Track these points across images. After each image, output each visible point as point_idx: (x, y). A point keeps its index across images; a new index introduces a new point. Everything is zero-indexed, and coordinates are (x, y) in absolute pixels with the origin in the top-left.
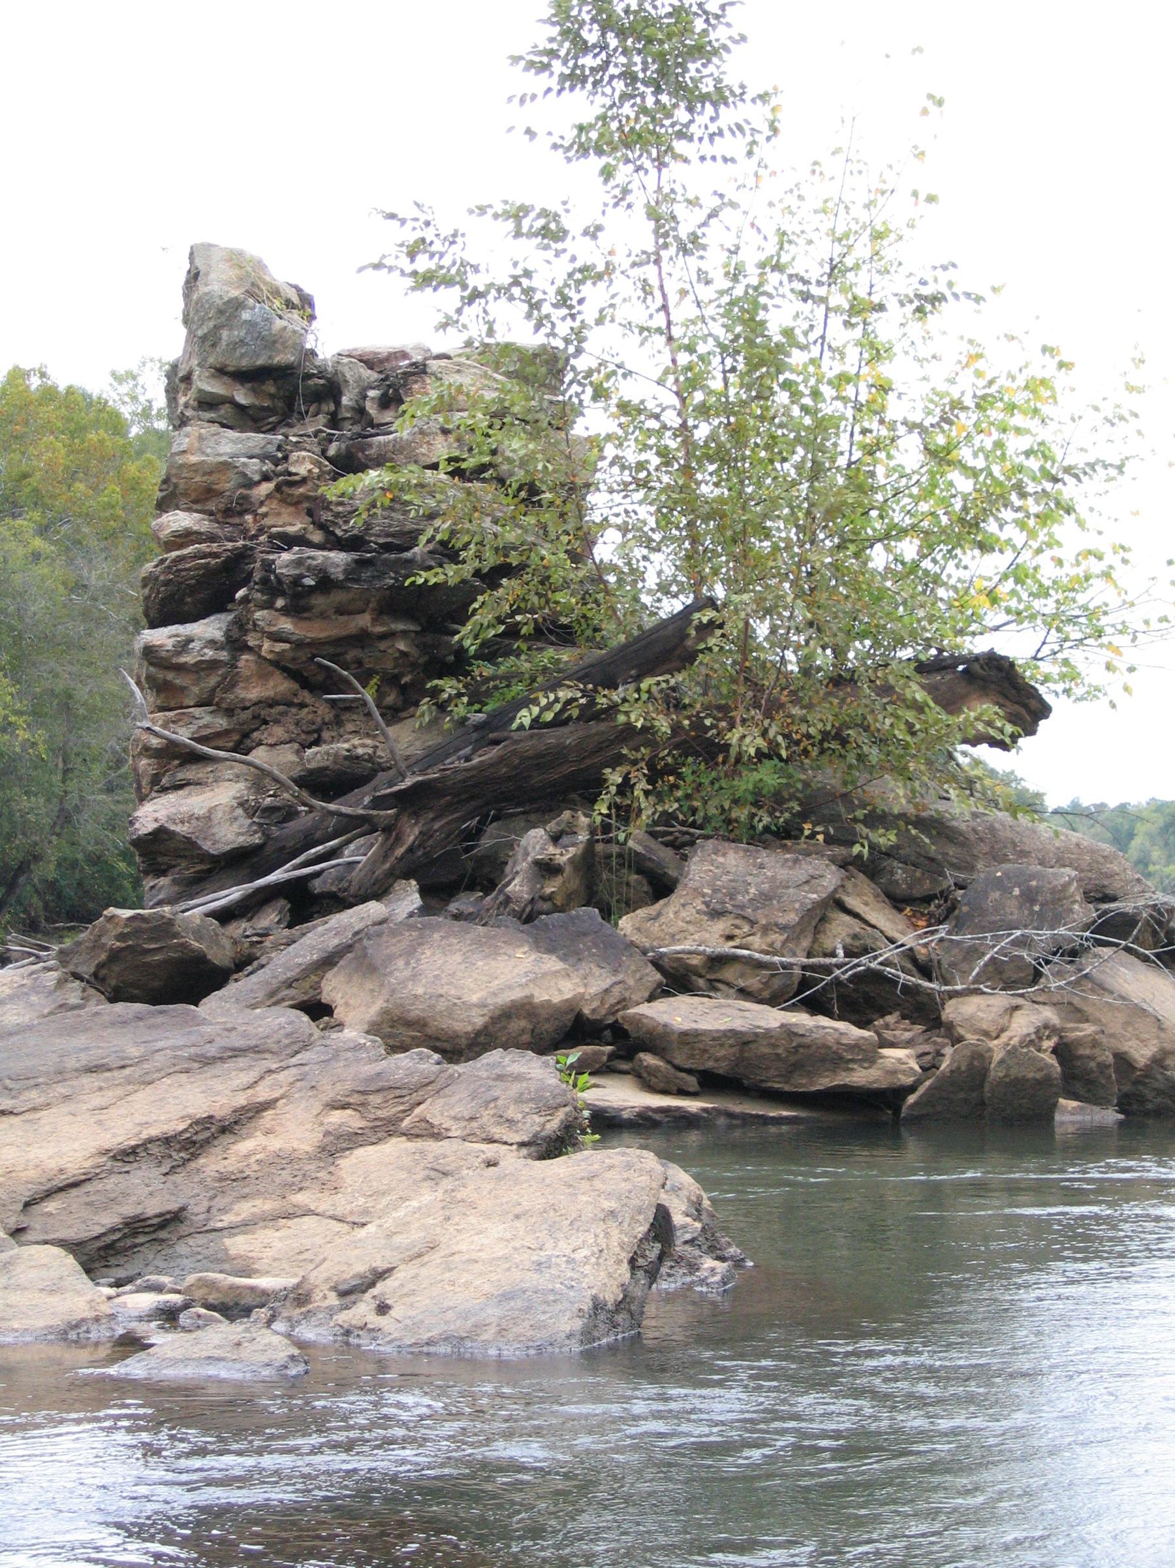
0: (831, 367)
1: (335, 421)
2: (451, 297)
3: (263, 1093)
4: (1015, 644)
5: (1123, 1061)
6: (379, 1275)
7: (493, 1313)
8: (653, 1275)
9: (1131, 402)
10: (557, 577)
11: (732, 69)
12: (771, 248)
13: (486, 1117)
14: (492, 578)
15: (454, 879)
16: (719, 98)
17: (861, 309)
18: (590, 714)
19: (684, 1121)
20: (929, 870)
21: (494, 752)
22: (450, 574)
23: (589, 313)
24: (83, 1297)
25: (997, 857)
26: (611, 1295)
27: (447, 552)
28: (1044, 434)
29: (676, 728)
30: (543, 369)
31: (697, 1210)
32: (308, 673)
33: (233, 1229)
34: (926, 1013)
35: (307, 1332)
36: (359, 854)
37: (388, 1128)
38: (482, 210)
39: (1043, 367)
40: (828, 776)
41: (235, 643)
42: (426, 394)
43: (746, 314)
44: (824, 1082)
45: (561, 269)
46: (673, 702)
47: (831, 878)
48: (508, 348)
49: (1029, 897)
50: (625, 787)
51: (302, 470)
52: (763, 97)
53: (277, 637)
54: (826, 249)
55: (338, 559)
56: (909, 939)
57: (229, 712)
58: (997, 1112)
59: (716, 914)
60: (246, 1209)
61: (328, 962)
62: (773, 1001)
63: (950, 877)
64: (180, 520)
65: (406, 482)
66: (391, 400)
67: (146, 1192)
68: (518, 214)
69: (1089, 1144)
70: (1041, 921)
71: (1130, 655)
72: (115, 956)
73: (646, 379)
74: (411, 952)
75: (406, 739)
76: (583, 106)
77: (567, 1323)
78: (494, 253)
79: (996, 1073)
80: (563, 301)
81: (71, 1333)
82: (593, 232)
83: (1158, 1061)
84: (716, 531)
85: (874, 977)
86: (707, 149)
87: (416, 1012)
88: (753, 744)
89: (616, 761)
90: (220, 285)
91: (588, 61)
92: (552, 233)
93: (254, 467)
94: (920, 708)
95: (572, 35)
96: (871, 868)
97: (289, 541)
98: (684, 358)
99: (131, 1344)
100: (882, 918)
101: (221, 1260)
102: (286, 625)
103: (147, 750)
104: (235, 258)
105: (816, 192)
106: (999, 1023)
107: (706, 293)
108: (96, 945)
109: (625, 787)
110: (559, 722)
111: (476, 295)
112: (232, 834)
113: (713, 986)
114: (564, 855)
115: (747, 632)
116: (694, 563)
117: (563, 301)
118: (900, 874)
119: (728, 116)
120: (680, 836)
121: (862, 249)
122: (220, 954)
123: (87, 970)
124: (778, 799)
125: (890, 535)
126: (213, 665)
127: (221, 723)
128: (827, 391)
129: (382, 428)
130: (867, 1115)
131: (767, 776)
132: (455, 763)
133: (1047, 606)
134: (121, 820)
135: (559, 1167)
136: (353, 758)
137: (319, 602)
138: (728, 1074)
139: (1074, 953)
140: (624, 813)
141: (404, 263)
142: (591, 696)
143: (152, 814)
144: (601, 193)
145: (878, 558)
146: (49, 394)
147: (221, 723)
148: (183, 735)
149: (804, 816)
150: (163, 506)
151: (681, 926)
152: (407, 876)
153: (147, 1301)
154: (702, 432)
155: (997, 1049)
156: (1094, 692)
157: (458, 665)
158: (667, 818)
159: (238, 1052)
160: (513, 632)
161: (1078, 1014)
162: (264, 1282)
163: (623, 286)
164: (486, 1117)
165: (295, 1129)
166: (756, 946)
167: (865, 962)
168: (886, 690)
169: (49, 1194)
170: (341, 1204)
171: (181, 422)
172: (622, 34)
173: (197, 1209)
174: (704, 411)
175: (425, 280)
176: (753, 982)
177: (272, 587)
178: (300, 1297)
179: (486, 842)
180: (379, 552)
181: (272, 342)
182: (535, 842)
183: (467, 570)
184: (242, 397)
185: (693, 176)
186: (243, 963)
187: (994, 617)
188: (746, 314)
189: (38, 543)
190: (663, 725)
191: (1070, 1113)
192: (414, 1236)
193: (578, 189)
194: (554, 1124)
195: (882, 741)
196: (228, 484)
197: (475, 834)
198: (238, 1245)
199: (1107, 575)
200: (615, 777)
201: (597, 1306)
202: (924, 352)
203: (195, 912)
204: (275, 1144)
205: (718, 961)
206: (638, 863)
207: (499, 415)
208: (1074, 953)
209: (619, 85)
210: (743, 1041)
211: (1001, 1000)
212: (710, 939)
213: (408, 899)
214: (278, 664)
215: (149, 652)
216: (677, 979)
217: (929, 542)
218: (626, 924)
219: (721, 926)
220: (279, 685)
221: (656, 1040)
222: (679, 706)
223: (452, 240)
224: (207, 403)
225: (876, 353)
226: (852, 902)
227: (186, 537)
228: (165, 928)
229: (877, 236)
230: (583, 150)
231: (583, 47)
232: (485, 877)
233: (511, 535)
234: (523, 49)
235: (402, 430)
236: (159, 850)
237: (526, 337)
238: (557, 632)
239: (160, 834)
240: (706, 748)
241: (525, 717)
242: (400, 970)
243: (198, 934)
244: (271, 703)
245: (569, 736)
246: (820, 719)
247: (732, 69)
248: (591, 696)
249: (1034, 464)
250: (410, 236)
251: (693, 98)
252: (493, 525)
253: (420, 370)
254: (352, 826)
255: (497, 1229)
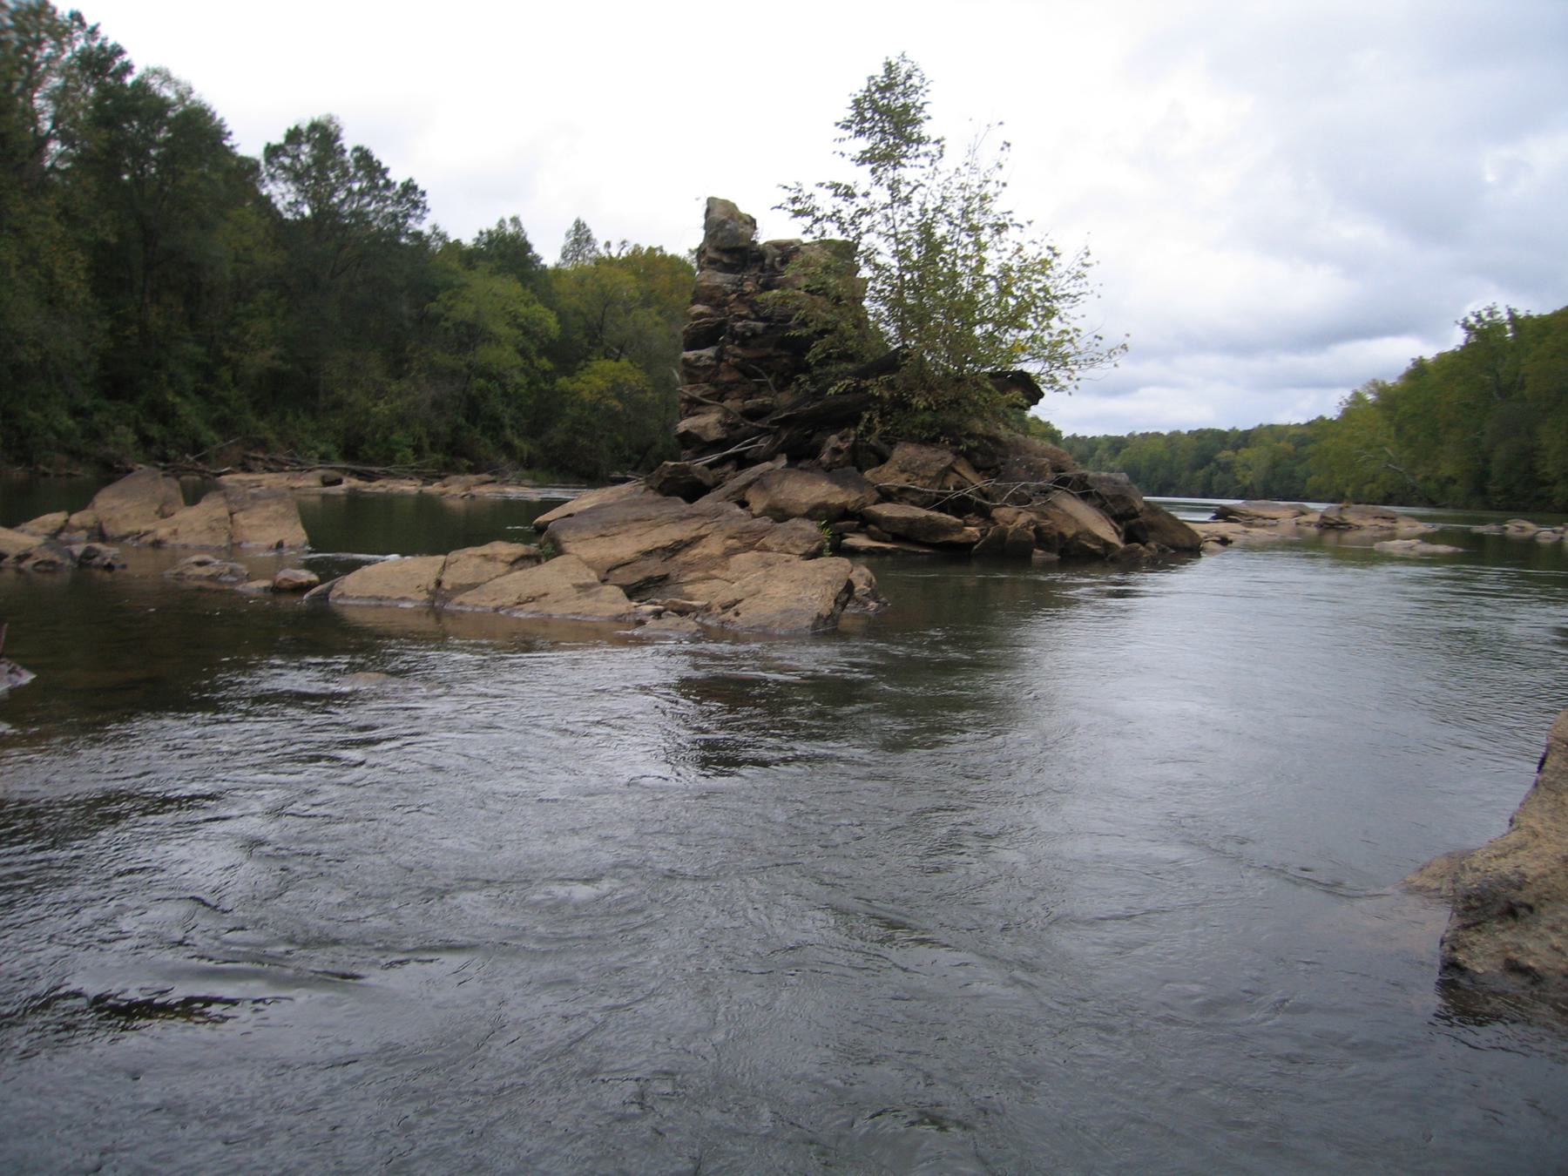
0: (961, 252)
1: (762, 270)
2: (808, 221)
3: (703, 532)
4: (1032, 368)
5: (1062, 535)
6: (738, 602)
7: (779, 617)
8: (844, 606)
9: (1084, 270)
10: (847, 334)
11: (926, 129)
12: (939, 203)
13: (788, 543)
14: (821, 333)
15: (801, 454)
16: (920, 141)
17: (974, 229)
18: (857, 389)
19: (883, 552)
20: (990, 457)
21: (818, 404)
22: (804, 332)
23: (863, 228)
24: (624, 605)
25: (1018, 453)
26: (826, 612)
27: (803, 323)
28: (1048, 283)
29: (892, 396)
30: (846, 251)
31: (870, 583)
32: (745, 370)
33: (687, 583)
34: (985, 513)
35: (709, 622)
36: (764, 443)
37: (749, 547)
38: (821, 185)
39: (1046, 254)
40: (951, 418)
41: (719, 358)
42: (798, 260)
43: (926, 230)
44: (941, 539)
45: (853, 209)
46: (891, 385)
47: (950, 458)
48: (831, 242)
49: (1029, 469)
50: (870, 420)
51: (748, 289)
52: (938, 142)
53: (735, 356)
54: (961, 204)
55: (760, 325)
56: (980, 484)
57: (716, 386)
58: (1009, 553)
59: (903, 471)
60: (692, 576)
61: (749, 485)
62: (924, 506)
63: (999, 460)
64: (699, 308)
65: (791, 293)
66: (784, 262)
67: (655, 568)
68: (835, 186)
69: (1047, 567)
70: (1033, 479)
71: (1078, 374)
72: (667, 480)
73: (886, 258)
74: (780, 482)
75: (785, 398)
76: (864, 144)
77: (807, 622)
78: (826, 202)
79: (1009, 538)
80: (853, 223)
81: (619, 619)
82: (866, 195)
83: (1076, 536)
84: (911, 317)
85: (965, 499)
86: (913, 161)
87: (781, 505)
88: (922, 404)
89: (867, 409)
90: (718, 215)
91: (867, 125)
92: (849, 194)
93: (729, 287)
94: (989, 391)
95: (860, 114)
96: (968, 455)
97: (741, 318)
98: (901, 247)
99: (641, 623)
100: (970, 475)
101: (681, 595)
102: (739, 351)
103: (683, 400)
104: (725, 203)
105: (956, 182)
106: (1014, 518)
107: (911, 220)
108: (660, 476)
109: (870, 420)
110: (845, 392)
111: (817, 221)
112: (714, 434)
113: (900, 500)
114: (844, 446)
115: (922, 359)
116: (903, 332)
117: (853, 223)
118: (979, 458)
119: (922, 149)
120: (891, 440)
121: (976, 204)
122: (709, 481)
123: (656, 485)
124: (931, 426)
125: (982, 322)
126: (709, 366)
127: (712, 390)
128: (959, 262)
129: (781, 273)
130: (960, 553)
131: (927, 417)
132: (803, 408)
133: (1046, 352)
134: (667, 427)
135: (812, 563)
136: (763, 405)
137: (753, 342)
138: (905, 534)
139: (1046, 492)
140: (869, 430)
141: (790, 206)
142: (858, 383)
143: (684, 425)
144: (870, 179)
145: (978, 331)
146: (664, 257)
147: (712, 390)
148: (697, 394)
149: (941, 434)
150: (693, 303)
151: (888, 476)
152: (782, 452)
153: (650, 608)
154: (908, 277)
155: (1011, 528)
156: (1062, 389)
157: (807, 369)
158: (886, 433)
159: (694, 516)
160: (829, 356)
161: (1046, 517)
162: (695, 603)
163: (877, 217)
164: (788, 543)
165: (713, 546)
166: (917, 485)
167: (961, 493)
168: (976, 384)
169: (618, 567)
170: (729, 575)
171: (701, 268)
172: (881, 115)
173: (673, 574)
174: (907, 268)
175: (798, 214)
176: (917, 499)
177: (734, 336)
178: (707, 609)
179: (815, 440)
180: (777, 322)
181: (738, 237)
182: (833, 440)
183: (811, 331)
184: (725, 259)
185: (909, 173)
186: (718, 484)
187: (1023, 357)
188: (926, 230)
189: (658, 318)
190: (887, 395)
191: (1038, 554)
192: (752, 587)
193: (861, 177)
194: (814, 547)
195: (975, 404)
196: (718, 294)
197: (810, 437)
198: (688, 589)
199: (1071, 341)
200: (866, 416)
201: (819, 616)
202: (1000, 247)
203: (700, 464)
204: (706, 551)
205: (903, 490)
206: (873, 449)
207: (826, 268)
208: (1046, 492)
209: (879, 135)
210: (911, 522)
211: (1013, 509)
212: (900, 481)
213: (782, 461)
214: (736, 366)
215: (685, 361)
216: (886, 496)
217: (998, 325)
218: (867, 474)
219: (905, 476)
220: (735, 375)
221: (877, 520)
222: (893, 388)
223: (810, 196)
224: (712, 262)
225: (981, 247)
226: (959, 469)
227: (701, 315)
228: (686, 470)
229: (983, 199)
230: (863, 163)
231: (864, 120)
232: (814, 453)
233: (829, 317)
234: (840, 120)
235: (788, 274)
236: (688, 439)
237: (837, 236)
238: (846, 357)
239: (687, 433)
240: (902, 405)
241: (832, 390)
242: (775, 489)
243: (700, 472)
244: (733, 382)
245: (848, 399)
246: (949, 396)
247: (926, 129)
248: (858, 383)
249: (1041, 294)
250: (793, 195)
251: (909, 141)
252: (823, 313)
253: (797, 250)
254: (762, 432)
255: (783, 586)
